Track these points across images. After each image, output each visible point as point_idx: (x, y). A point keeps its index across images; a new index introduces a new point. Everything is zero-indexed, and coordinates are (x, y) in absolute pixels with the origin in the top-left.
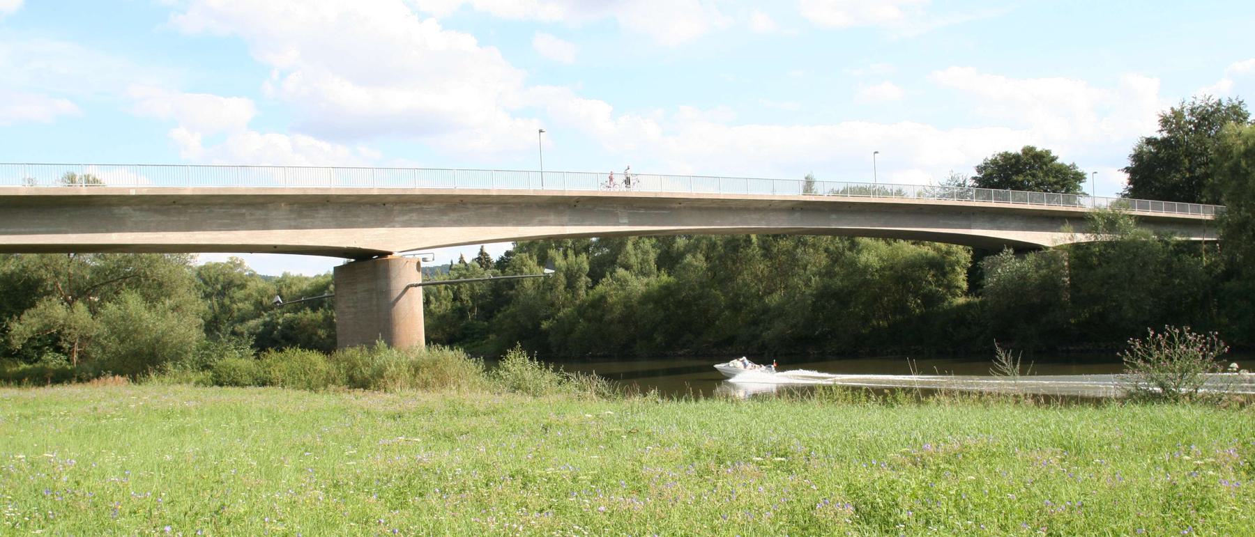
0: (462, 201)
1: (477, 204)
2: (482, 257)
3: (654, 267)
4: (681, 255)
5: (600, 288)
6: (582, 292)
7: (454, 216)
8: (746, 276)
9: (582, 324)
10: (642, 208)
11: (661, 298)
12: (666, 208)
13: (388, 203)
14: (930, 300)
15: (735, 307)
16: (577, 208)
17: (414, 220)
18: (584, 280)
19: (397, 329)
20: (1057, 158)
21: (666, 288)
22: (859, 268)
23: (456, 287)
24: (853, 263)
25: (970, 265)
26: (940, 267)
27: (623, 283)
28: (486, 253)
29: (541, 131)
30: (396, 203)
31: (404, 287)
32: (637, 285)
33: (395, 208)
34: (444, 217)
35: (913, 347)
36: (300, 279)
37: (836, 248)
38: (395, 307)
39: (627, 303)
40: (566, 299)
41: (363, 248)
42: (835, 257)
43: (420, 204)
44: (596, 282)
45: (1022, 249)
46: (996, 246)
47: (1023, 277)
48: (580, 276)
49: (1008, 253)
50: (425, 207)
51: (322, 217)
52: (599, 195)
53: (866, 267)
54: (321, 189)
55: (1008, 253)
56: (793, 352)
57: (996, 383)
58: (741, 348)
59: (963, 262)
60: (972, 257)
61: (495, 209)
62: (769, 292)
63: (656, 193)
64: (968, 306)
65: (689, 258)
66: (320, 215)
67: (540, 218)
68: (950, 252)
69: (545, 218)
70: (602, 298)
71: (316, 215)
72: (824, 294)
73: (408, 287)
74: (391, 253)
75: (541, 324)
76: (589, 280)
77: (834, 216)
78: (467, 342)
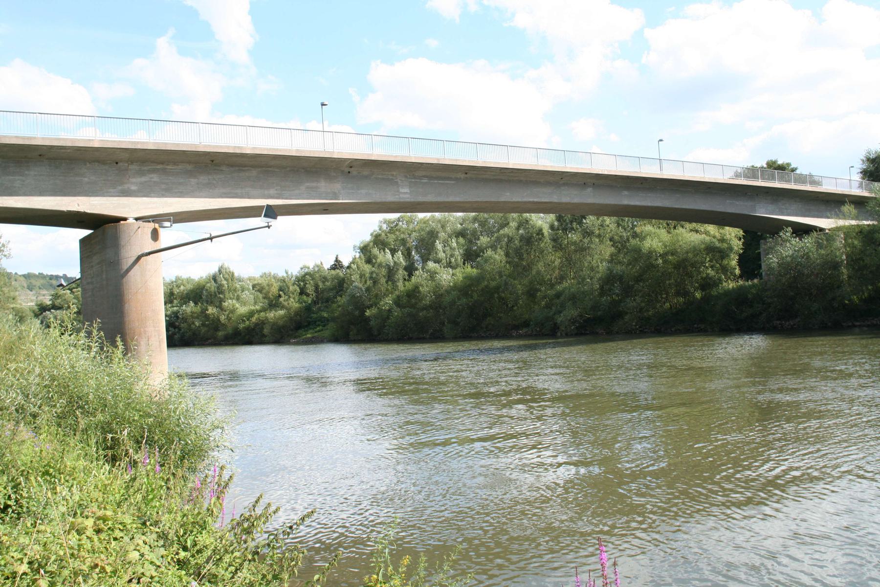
0: (212, 161)
1: (232, 166)
2: (337, 264)
3: (460, 259)
4: (482, 250)
5: (414, 279)
6: (400, 284)
7: (203, 179)
8: (540, 266)
9: (397, 312)
10: (424, 176)
11: (466, 288)
12: (451, 178)
13: (121, 161)
14: (707, 284)
15: (531, 293)
16: (350, 174)
17: (154, 182)
18: (401, 273)
19: (126, 305)
20: (796, 169)
21: (468, 278)
22: (644, 254)
23: (302, 284)
24: (638, 250)
25: (742, 252)
26: (717, 252)
27: (432, 275)
28: (340, 261)
29: (323, 105)
30: (131, 161)
31: (134, 259)
32: (446, 277)
33: (131, 167)
34: (192, 180)
35: (696, 326)
36: (189, 280)
37: (621, 237)
38: (124, 280)
39: (439, 294)
40: (387, 290)
41: (89, 211)
42: (620, 245)
43: (162, 163)
44: (410, 275)
45: (802, 231)
46: (776, 227)
47: (807, 256)
48: (398, 269)
49: (787, 233)
50: (169, 167)
51: (35, 175)
52: (373, 159)
53: (651, 252)
54: (23, 138)
55: (787, 233)
56: (583, 332)
57: (541, 343)
58: (536, 330)
59: (736, 248)
60: (743, 244)
61: (254, 173)
62: (562, 278)
63: (438, 159)
64: (740, 290)
65: (489, 252)
66: (32, 173)
67: (308, 184)
68: (724, 240)
69: (314, 184)
70: (416, 288)
71: (26, 172)
72: (610, 279)
73: (139, 258)
74: (125, 219)
75: (366, 311)
76: (406, 273)
77: (626, 193)
78: (311, 329)
